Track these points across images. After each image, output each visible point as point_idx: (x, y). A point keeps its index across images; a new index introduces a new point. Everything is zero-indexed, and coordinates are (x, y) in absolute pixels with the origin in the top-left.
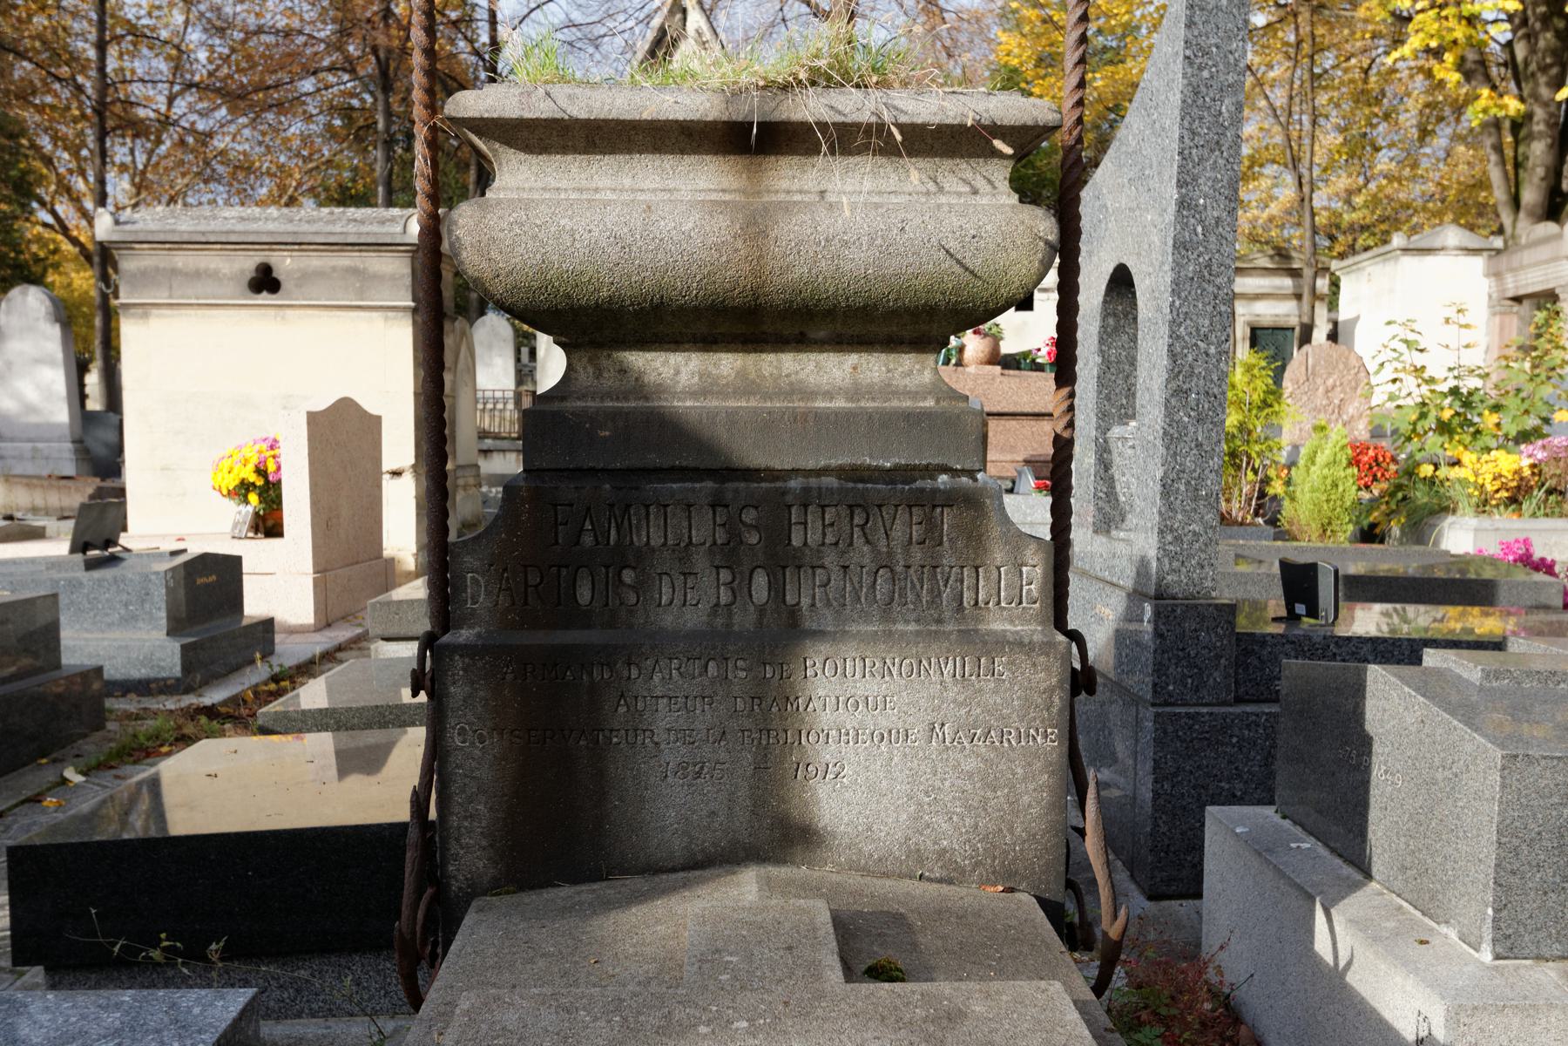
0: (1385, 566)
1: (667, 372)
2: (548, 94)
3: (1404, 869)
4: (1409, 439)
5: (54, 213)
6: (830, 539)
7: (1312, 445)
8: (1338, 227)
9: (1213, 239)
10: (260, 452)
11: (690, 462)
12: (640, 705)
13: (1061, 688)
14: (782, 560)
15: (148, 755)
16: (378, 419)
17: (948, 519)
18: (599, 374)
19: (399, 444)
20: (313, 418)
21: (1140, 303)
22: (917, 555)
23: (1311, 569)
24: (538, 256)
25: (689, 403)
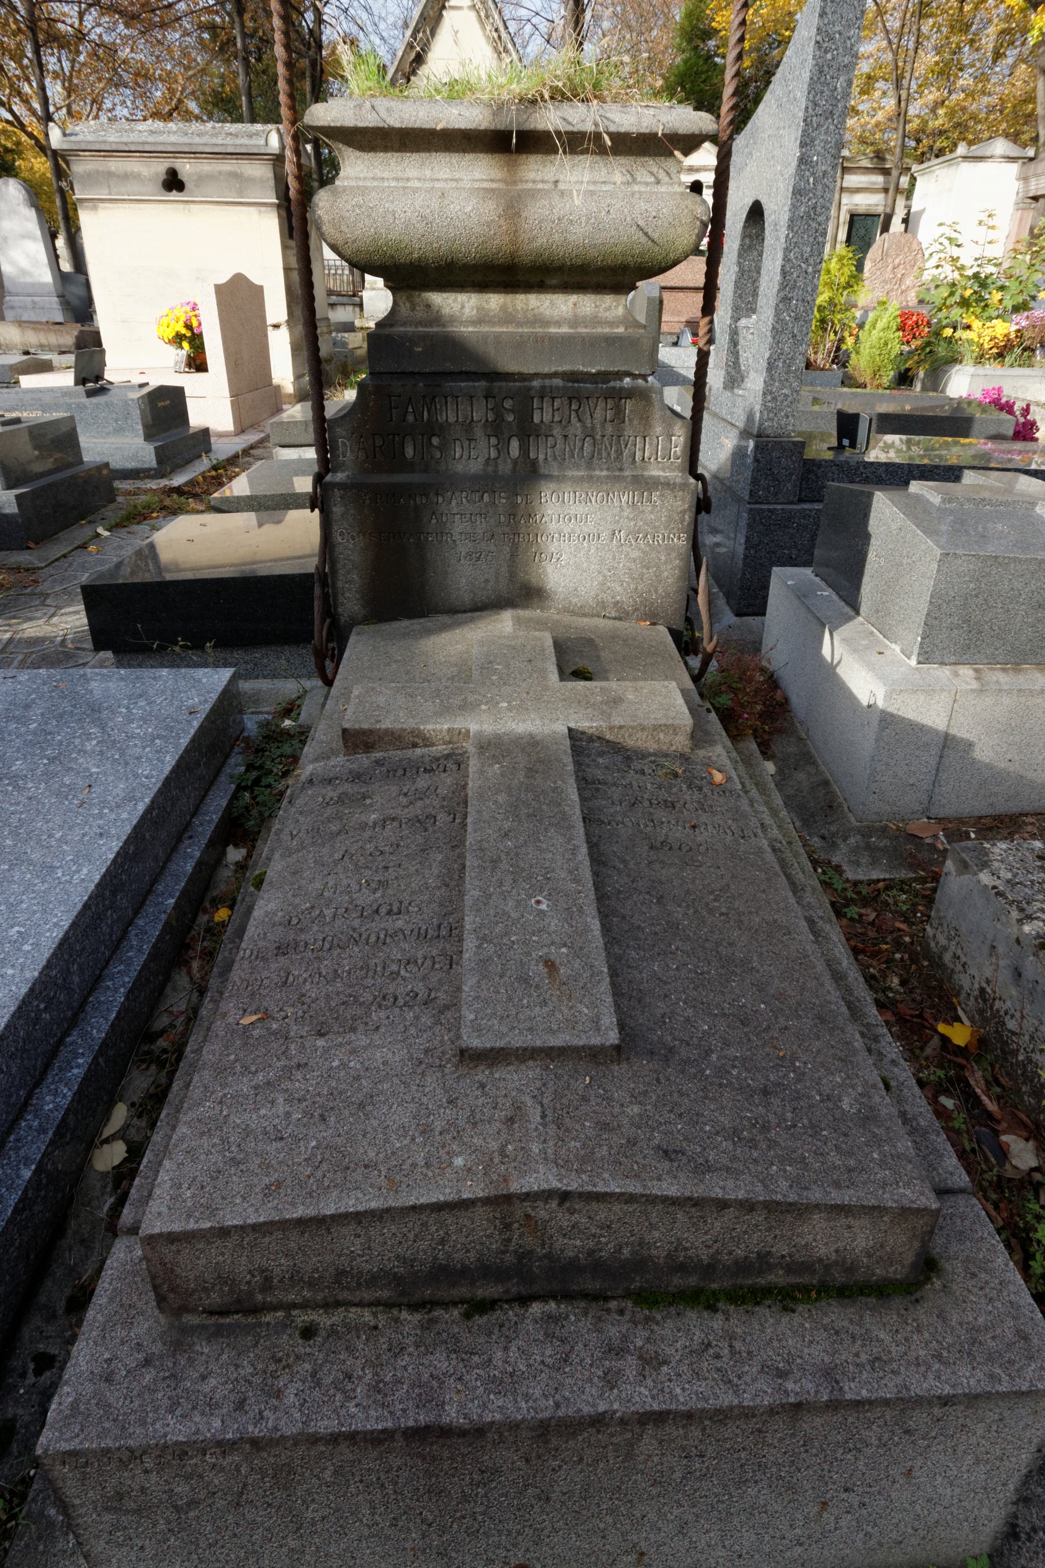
0: (908, 407)
1: (456, 307)
2: (373, 107)
3: (877, 611)
4: (940, 310)
5: (11, 111)
6: (557, 418)
7: (877, 305)
8: (924, 132)
9: (820, 187)
11: (472, 368)
14: (528, 431)
15: (145, 519)
16: (261, 287)
17: (629, 406)
18: (413, 309)
19: (276, 306)
20: (218, 288)
21: (767, 232)
22: (609, 429)
23: (855, 417)
25: (470, 329)
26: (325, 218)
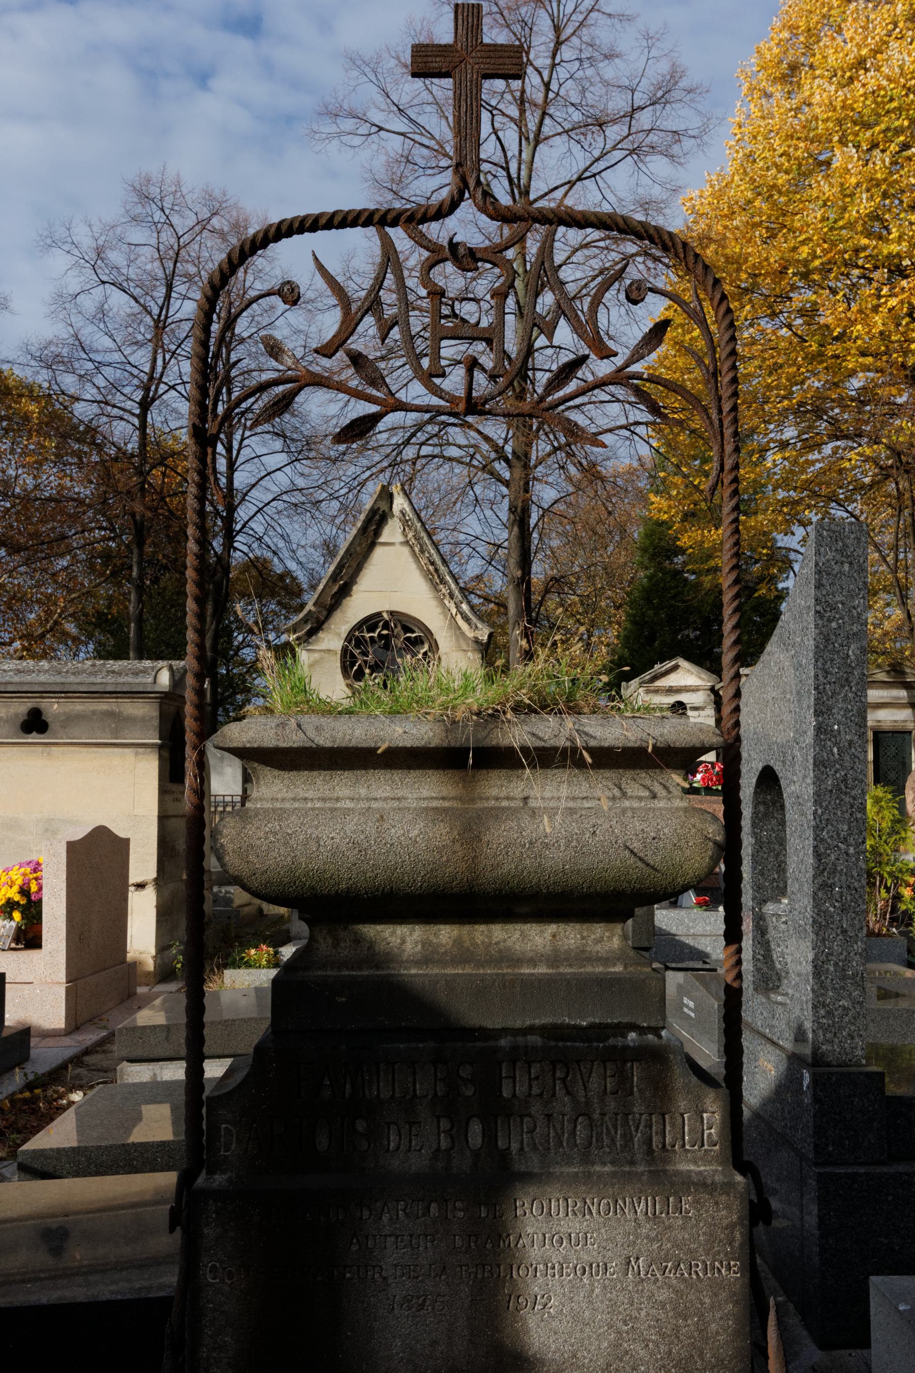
1: (395, 941)
2: (299, 726)
6: (535, 1091)
9: (847, 758)
10: (24, 875)
12: (370, 1243)
13: (742, 1224)
14: (496, 1111)
16: (127, 841)
18: (336, 945)
19: (143, 863)
20: (72, 847)
24: (289, 859)
25: (413, 971)
26: (229, 847)
